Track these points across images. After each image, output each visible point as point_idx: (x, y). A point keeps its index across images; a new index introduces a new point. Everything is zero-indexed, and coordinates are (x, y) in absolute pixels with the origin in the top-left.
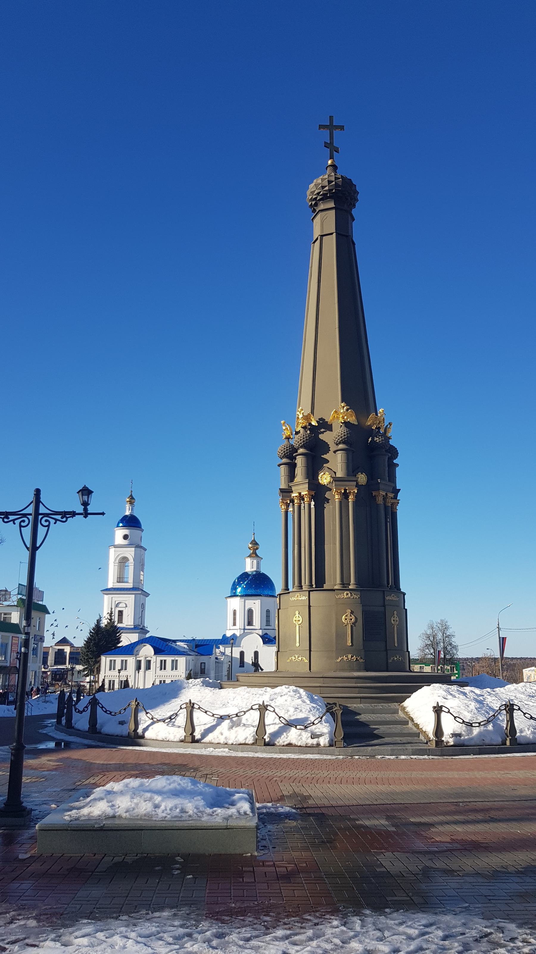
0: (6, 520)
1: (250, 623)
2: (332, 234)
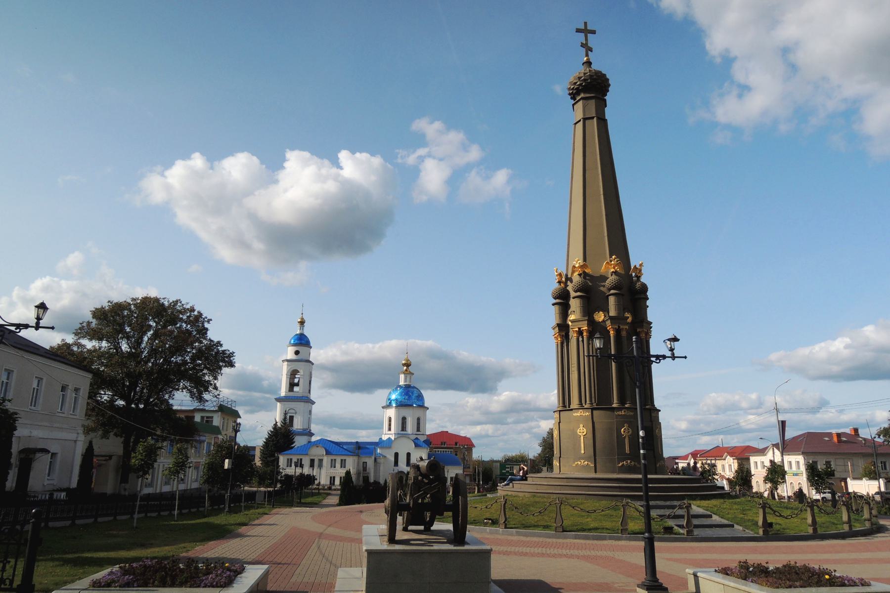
1: (404, 428)
2: (593, 118)
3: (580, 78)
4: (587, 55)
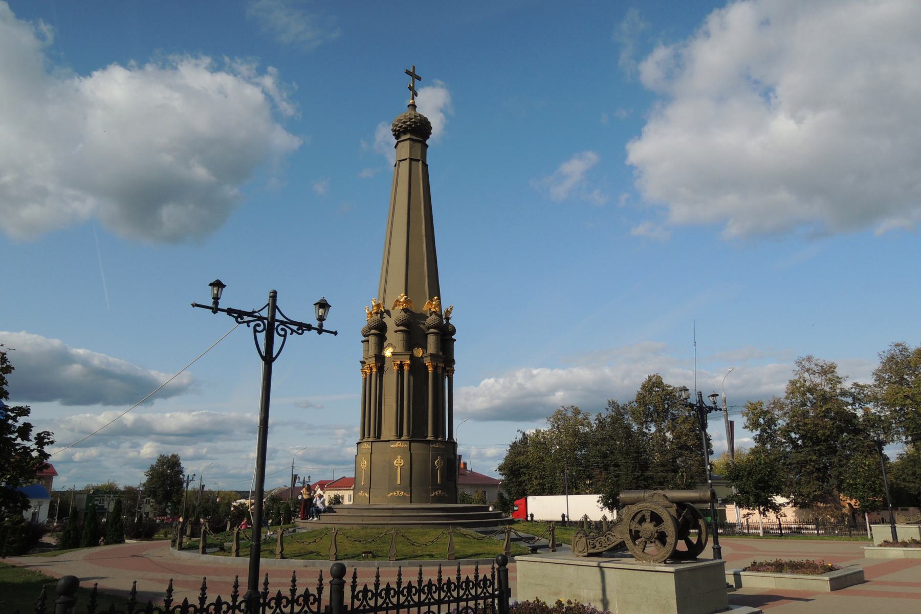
0: (239, 320)
2: (418, 161)
3: (410, 119)
4: (413, 99)
